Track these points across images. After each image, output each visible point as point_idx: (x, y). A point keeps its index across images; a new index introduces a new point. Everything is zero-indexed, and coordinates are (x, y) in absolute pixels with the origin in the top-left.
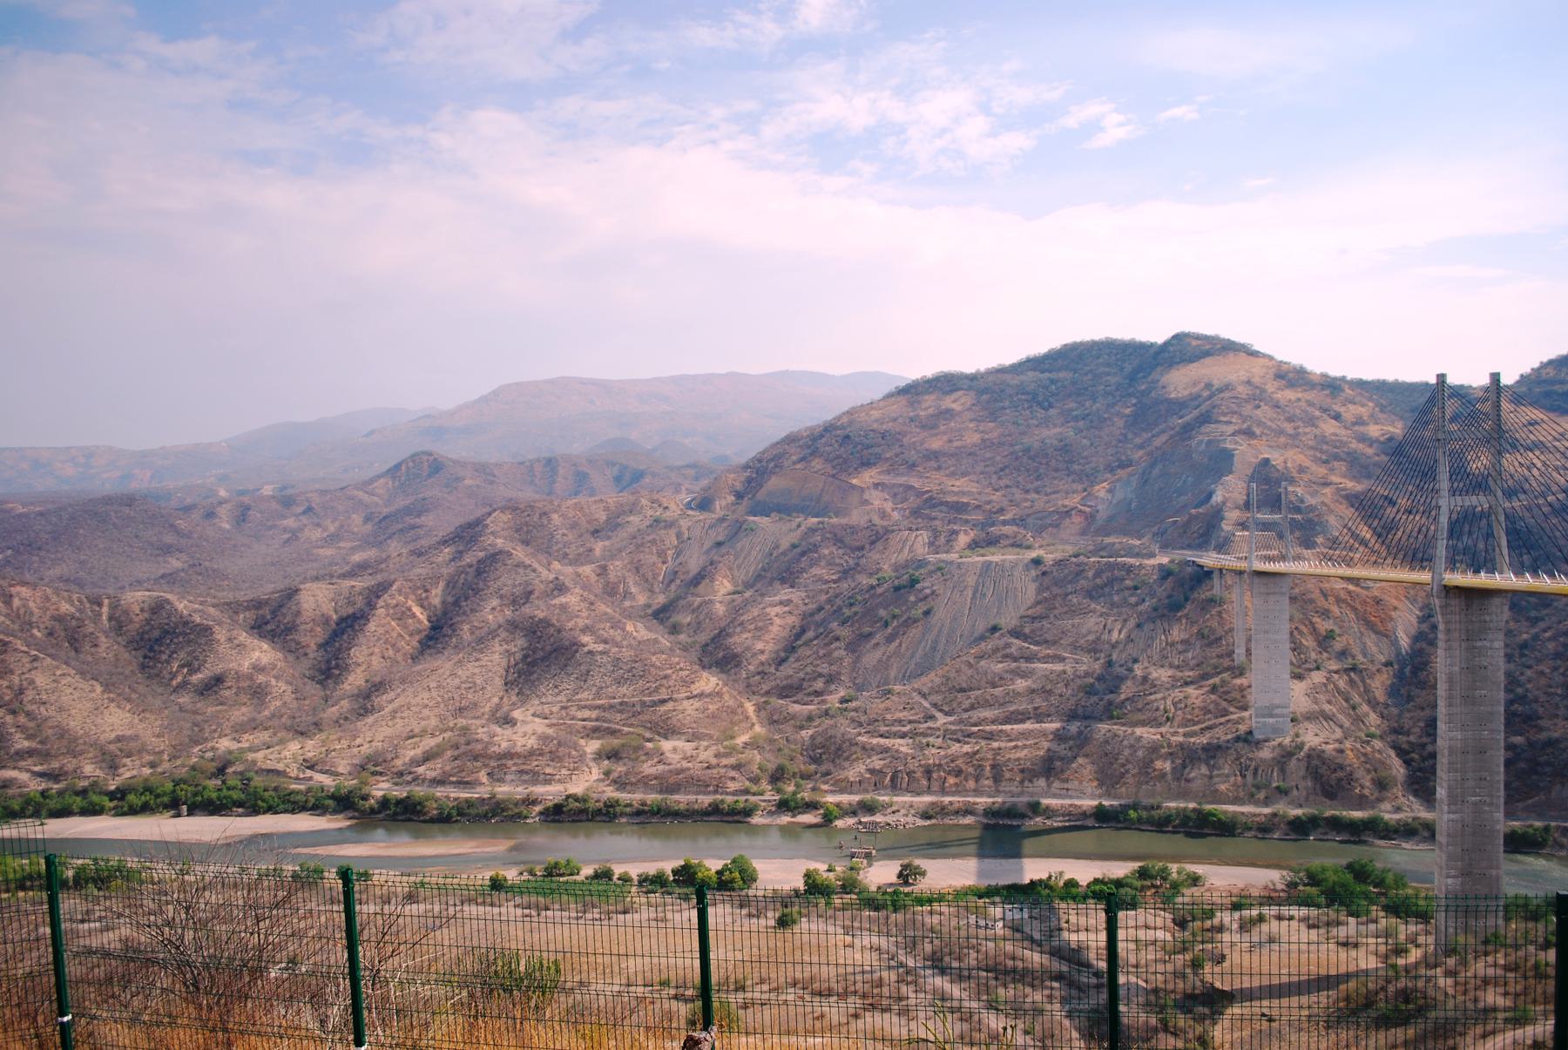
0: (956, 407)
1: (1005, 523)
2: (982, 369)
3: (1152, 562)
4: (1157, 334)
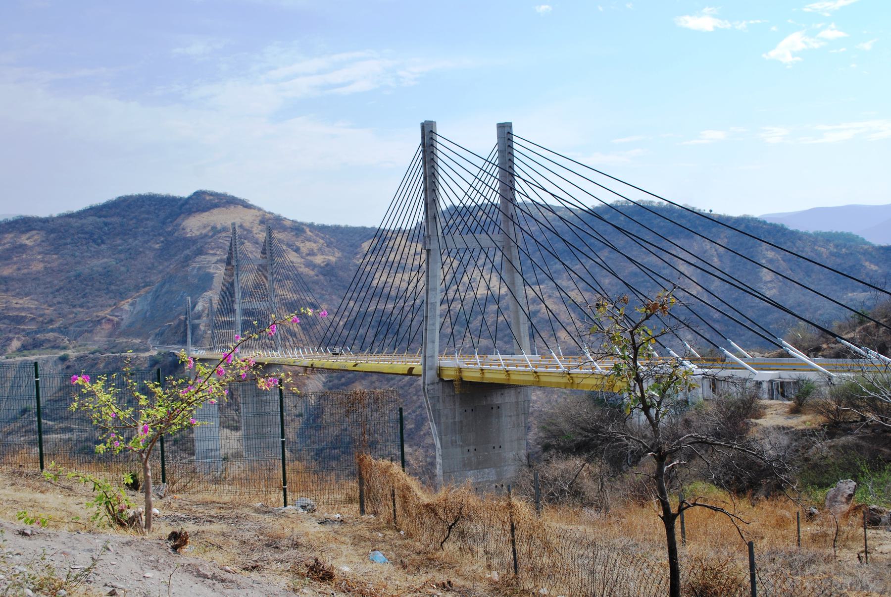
0: (29, 243)
1: (52, 330)
2: (55, 215)
3: (147, 354)
4: (184, 192)
